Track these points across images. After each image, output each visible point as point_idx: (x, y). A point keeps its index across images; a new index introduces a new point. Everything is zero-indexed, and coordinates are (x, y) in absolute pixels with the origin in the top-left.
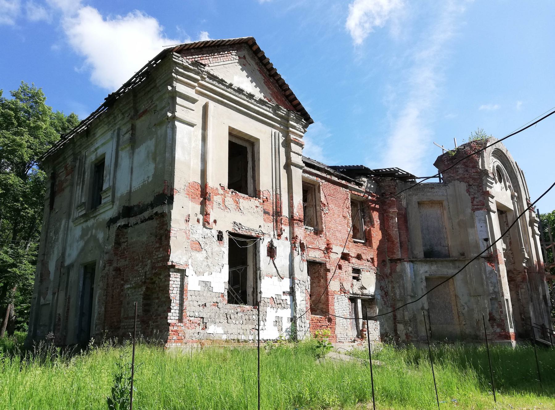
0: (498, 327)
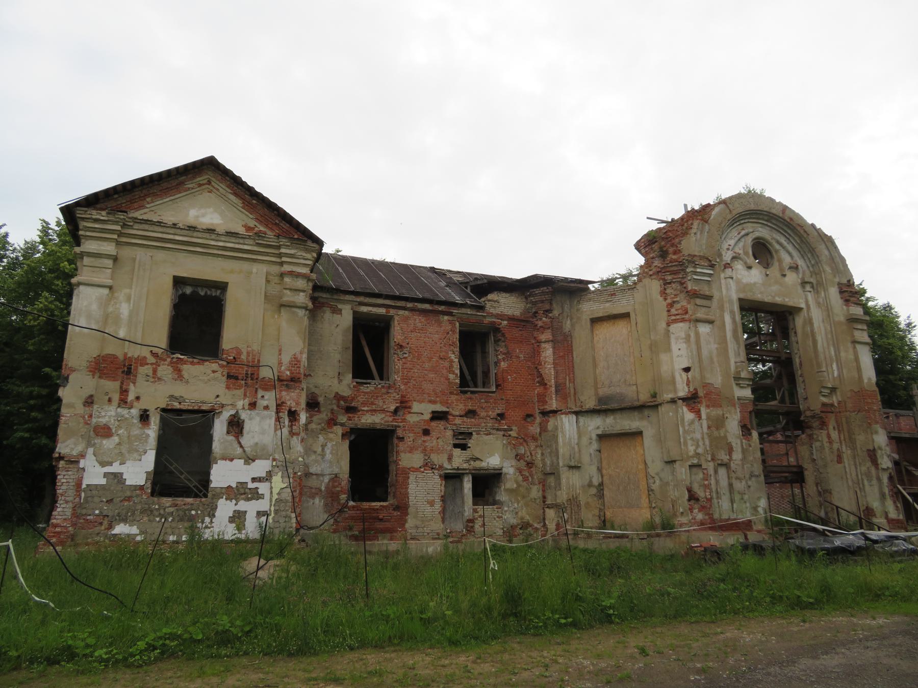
0: (700, 511)
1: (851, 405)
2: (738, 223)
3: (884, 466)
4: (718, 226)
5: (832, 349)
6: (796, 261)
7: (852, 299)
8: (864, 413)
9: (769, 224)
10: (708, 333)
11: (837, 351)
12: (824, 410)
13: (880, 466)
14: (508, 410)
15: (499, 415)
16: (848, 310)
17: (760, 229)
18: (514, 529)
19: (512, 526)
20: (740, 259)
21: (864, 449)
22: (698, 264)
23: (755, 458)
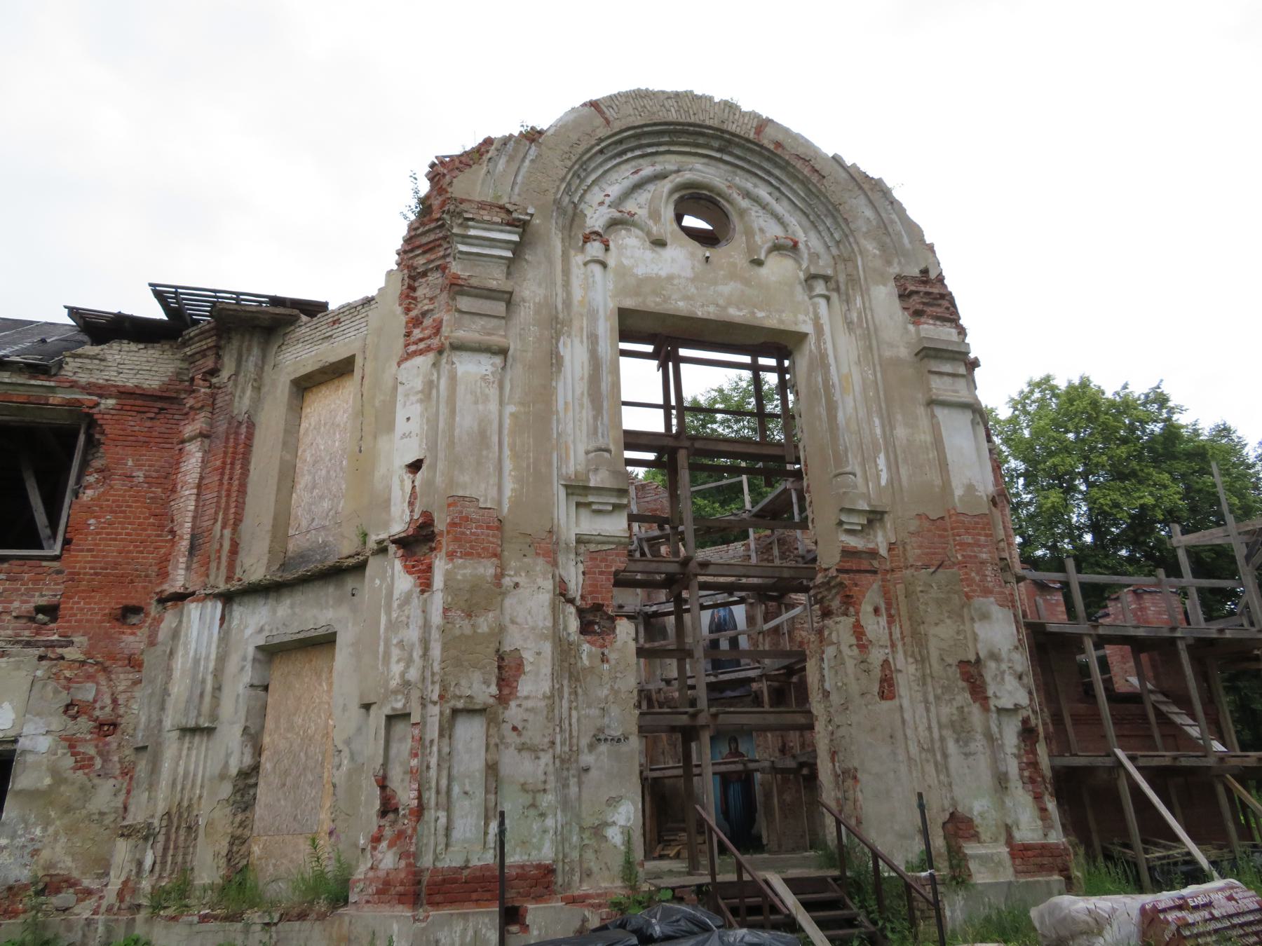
1: (918, 551)
2: (638, 153)
3: (1006, 702)
4: (567, 149)
5: (877, 421)
6: (794, 233)
7: (929, 310)
8: (955, 569)
9: (726, 158)
10: (484, 378)
11: (889, 424)
12: (847, 565)
13: (993, 703)
14: (70, 598)
15: (39, 609)
16: (918, 332)
17: (698, 166)
18: (15, 895)
19: (10, 888)
20: (634, 224)
21: (950, 660)
22: (472, 219)
23: (616, 692)
